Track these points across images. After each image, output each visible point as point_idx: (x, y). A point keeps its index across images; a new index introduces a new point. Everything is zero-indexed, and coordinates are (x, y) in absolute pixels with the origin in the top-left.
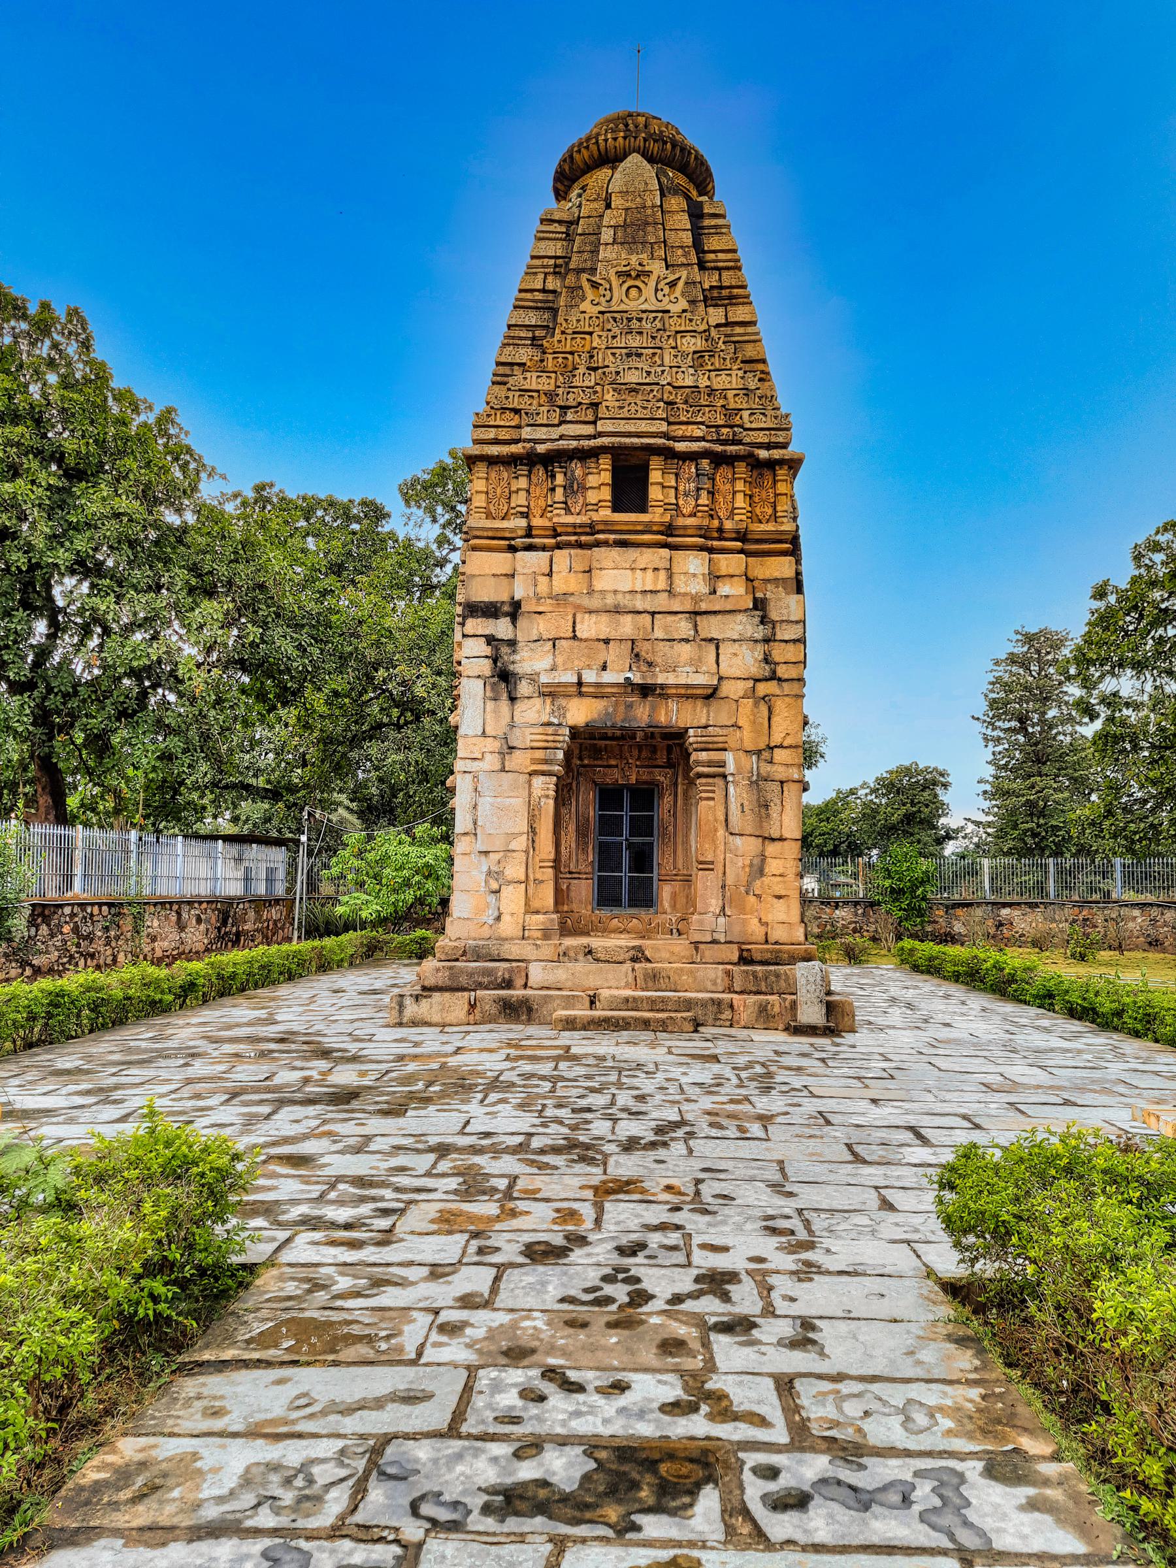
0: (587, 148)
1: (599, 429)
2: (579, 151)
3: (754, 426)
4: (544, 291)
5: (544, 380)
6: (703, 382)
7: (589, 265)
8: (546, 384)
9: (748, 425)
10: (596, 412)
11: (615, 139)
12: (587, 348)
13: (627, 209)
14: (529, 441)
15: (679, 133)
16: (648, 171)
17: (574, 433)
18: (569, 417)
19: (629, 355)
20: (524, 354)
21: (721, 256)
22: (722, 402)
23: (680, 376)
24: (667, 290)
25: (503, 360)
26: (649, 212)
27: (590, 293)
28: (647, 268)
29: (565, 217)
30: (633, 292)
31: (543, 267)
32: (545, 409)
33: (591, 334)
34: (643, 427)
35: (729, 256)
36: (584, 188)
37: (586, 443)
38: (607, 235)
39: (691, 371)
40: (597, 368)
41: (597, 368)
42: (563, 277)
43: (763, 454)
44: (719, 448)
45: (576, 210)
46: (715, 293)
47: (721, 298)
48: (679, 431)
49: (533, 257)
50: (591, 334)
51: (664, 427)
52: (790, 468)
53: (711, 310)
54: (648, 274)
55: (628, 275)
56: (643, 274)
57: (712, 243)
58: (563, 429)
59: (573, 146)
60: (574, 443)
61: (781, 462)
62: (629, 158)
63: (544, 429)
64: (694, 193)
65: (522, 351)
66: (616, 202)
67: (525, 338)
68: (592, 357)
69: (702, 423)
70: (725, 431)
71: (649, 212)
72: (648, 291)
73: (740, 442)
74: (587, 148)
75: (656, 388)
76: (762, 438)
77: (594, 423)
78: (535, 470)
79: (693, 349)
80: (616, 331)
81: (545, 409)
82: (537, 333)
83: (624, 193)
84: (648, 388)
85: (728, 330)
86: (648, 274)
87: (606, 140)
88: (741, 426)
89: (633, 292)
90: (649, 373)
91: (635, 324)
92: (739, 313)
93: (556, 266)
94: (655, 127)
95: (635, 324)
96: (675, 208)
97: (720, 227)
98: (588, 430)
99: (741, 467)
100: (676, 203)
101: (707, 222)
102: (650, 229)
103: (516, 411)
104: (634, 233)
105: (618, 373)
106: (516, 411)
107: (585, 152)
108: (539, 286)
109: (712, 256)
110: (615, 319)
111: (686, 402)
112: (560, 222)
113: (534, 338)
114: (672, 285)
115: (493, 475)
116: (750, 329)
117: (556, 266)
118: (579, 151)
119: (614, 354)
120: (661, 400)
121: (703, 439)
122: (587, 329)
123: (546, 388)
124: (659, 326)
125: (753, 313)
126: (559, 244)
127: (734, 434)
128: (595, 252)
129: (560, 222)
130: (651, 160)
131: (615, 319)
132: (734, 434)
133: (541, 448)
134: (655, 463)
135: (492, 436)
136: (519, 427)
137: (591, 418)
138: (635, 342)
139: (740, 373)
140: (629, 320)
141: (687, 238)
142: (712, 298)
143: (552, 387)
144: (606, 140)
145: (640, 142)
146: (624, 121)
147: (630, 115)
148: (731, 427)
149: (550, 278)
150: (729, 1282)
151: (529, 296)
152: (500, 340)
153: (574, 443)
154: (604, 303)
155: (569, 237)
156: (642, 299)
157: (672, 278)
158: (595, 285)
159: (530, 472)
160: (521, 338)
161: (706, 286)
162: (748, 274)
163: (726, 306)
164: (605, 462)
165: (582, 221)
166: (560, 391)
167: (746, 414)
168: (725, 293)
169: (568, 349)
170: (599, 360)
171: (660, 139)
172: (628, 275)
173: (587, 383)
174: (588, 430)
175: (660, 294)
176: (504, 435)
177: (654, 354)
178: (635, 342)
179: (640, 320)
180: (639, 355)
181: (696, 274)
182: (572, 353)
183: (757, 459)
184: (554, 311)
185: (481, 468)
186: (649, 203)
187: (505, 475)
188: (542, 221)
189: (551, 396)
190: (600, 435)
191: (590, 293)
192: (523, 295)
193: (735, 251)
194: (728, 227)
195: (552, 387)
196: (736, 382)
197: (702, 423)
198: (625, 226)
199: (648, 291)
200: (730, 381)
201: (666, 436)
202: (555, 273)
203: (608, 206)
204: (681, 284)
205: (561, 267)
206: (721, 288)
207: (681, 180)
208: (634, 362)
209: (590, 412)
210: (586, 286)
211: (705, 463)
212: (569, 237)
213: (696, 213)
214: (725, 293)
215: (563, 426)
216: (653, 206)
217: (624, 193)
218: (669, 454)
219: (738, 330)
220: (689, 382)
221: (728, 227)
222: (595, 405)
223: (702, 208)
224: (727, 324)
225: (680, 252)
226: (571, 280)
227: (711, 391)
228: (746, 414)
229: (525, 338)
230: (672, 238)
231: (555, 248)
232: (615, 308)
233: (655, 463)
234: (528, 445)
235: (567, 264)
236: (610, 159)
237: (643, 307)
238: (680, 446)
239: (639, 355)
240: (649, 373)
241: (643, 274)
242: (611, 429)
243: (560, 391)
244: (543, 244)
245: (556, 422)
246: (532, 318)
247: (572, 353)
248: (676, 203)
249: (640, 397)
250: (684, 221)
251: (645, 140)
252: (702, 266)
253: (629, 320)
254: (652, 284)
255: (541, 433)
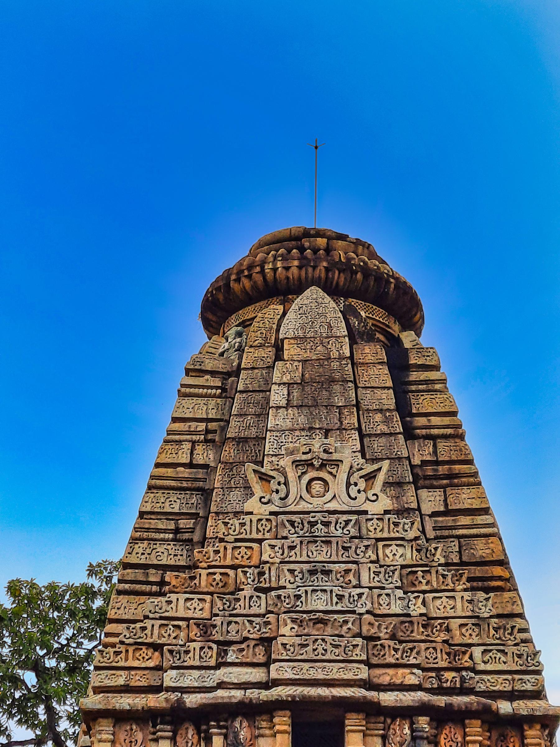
0: (249, 277)
1: (274, 675)
2: (238, 280)
3: (489, 667)
4: (191, 465)
5: (195, 603)
6: (417, 609)
7: (253, 432)
8: (199, 609)
9: (482, 667)
10: (268, 653)
11: (287, 269)
12: (255, 561)
13: (304, 361)
14: (174, 689)
15: (373, 255)
16: (331, 307)
17: (237, 679)
18: (231, 657)
19: (312, 572)
20: (167, 554)
21: (435, 421)
22: (443, 636)
23: (384, 600)
24: (362, 484)
25: (133, 560)
26: (335, 365)
27: (258, 488)
28: (335, 456)
29: (220, 365)
30: (317, 487)
31: (190, 433)
32: (197, 645)
33: (260, 541)
34: (335, 672)
35: (446, 420)
36: (246, 324)
37: (253, 694)
38: (278, 396)
39: (400, 593)
40: (271, 589)
41: (271, 589)
42: (219, 446)
43: (505, 707)
44: (441, 701)
45: (234, 356)
46: (429, 471)
47: (437, 477)
48: (385, 677)
49: (175, 420)
50: (260, 541)
51: (363, 673)
52: (544, 727)
53: (423, 493)
54: (337, 463)
55: (309, 464)
56: (329, 464)
57: (422, 403)
58: (222, 674)
59: (228, 272)
60: (238, 694)
61: (532, 719)
62: (307, 293)
63: (196, 673)
64: (395, 328)
65: (161, 549)
66: (289, 350)
67: (165, 531)
68: (261, 574)
69: (417, 666)
70: (449, 675)
71: (335, 365)
72: (338, 485)
73: (470, 691)
74: (249, 277)
75: (351, 618)
76: (501, 684)
77: (266, 665)
78: (182, 731)
79: (401, 562)
80: (294, 539)
81: (197, 645)
82: (183, 523)
83: (300, 340)
84: (340, 618)
85: (448, 520)
86: (337, 463)
87: (275, 270)
88: (473, 670)
89: (317, 487)
90: (340, 597)
91: (320, 530)
92: (464, 498)
93: (207, 431)
94: (341, 252)
95: (320, 530)
96: (370, 358)
97: (433, 382)
98: (256, 675)
99: (475, 728)
100: (371, 352)
101: (414, 376)
102: (337, 388)
103: (157, 647)
104: (315, 390)
105: (298, 597)
106: (157, 647)
107: (246, 283)
108: (185, 459)
109: (421, 421)
110: (292, 523)
111: (393, 637)
112: (213, 373)
113: (177, 531)
114: (370, 477)
115: (122, 736)
116: (480, 519)
117: (207, 431)
118: (238, 280)
119: (292, 571)
120: (359, 635)
121: (418, 688)
122: (254, 536)
123: (198, 614)
124: (353, 532)
125: (483, 498)
126: (212, 403)
127: (463, 680)
128: (262, 415)
129: (213, 373)
130: (333, 291)
131: (292, 523)
132: (463, 680)
133: (192, 700)
134: (353, 722)
135: (121, 681)
136: (159, 668)
137: (261, 658)
138: (321, 554)
139: (467, 595)
140: (312, 524)
141: (388, 399)
142: (426, 477)
143: (206, 614)
144: (275, 270)
145: (321, 271)
146: (296, 240)
147: (307, 234)
148: (458, 670)
149: (199, 449)
150: (258, 289)
151: (169, 472)
152: (128, 532)
153: (238, 694)
154: (277, 502)
155: (226, 393)
156: (329, 496)
157: (370, 468)
158: (265, 478)
159: (175, 733)
160: (158, 531)
161: (416, 461)
162: (473, 443)
163: (444, 487)
164: (283, 721)
165: (243, 374)
166: (218, 621)
167: (477, 652)
168: (442, 470)
169: (228, 562)
170: (271, 578)
171: (346, 267)
172: (309, 464)
173: (255, 610)
174: (256, 675)
175: (353, 491)
176: (138, 680)
177: (347, 571)
178: (321, 554)
179: (327, 524)
180: (327, 573)
181: (401, 446)
182: (234, 567)
183: (496, 714)
184: (206, 494)
185: (105, 729)
186: (335, 354)
187: (139, 736)
188: (188, 372)
189: (205, 627)
190: (276, 683)
191: (258, 488)
192: (162, 471)
193: (454, 414)
194: (443, 381)
195: (206, 614)
196: (461, 608)
197: (417, 666)
198: (303, 383)
199: (338, 485)
200: (455, 605)
201: (368, 685)
202: (206, 441)
203: (279, 357)
204: (381, 477)
205: (215, 436)
206: (437, 463)
207: (379, 315)
208: (320, 581)
209: (260, 649)
210: (253, 479)
211: (423, 722)
212: (226, 393)
213: (398, 363)
214: (442, 470)
215: (223, 670)
216: (341, 358)
217: (300, 340)
218: (371, 711)
219: (465, 520)
220: (396, 608)
221: (443, 381)
222: (266, 642)
223: (407, 357)
224: (447, 513)
225: (378, 417)
226: (229, 452)
227: (428, 621)
228: (477, 652)
229: (165, 531)
230: (368, 399)
231: (208, 408)
232: (292, 508)
233: (353, 722)
234: (174, 697)
235: (224, 429)
236: (283, 291)
237: (333, 506)
238: (388, 698)
239: (327, 573)
240: (340, 597)
241: (329, 464)
242: (289, 675)
243: (218, 621)
244: (188, 402)
245: (213, 663)
246: (174, 503)
247: (234, 567)
248: (371, 352)
249: (329, 630)
250: (382, 376)
251: (327, 270)
252: (409, 434)
253: (312, 524)
254: (342, 476)
255: (191, 679)
